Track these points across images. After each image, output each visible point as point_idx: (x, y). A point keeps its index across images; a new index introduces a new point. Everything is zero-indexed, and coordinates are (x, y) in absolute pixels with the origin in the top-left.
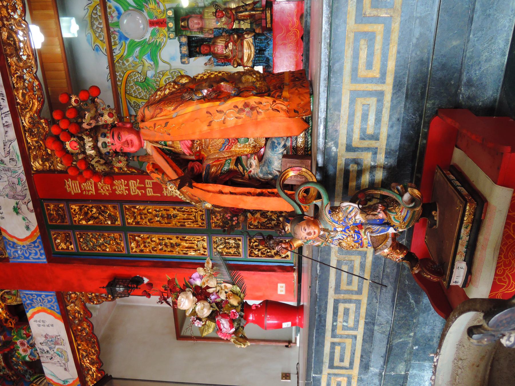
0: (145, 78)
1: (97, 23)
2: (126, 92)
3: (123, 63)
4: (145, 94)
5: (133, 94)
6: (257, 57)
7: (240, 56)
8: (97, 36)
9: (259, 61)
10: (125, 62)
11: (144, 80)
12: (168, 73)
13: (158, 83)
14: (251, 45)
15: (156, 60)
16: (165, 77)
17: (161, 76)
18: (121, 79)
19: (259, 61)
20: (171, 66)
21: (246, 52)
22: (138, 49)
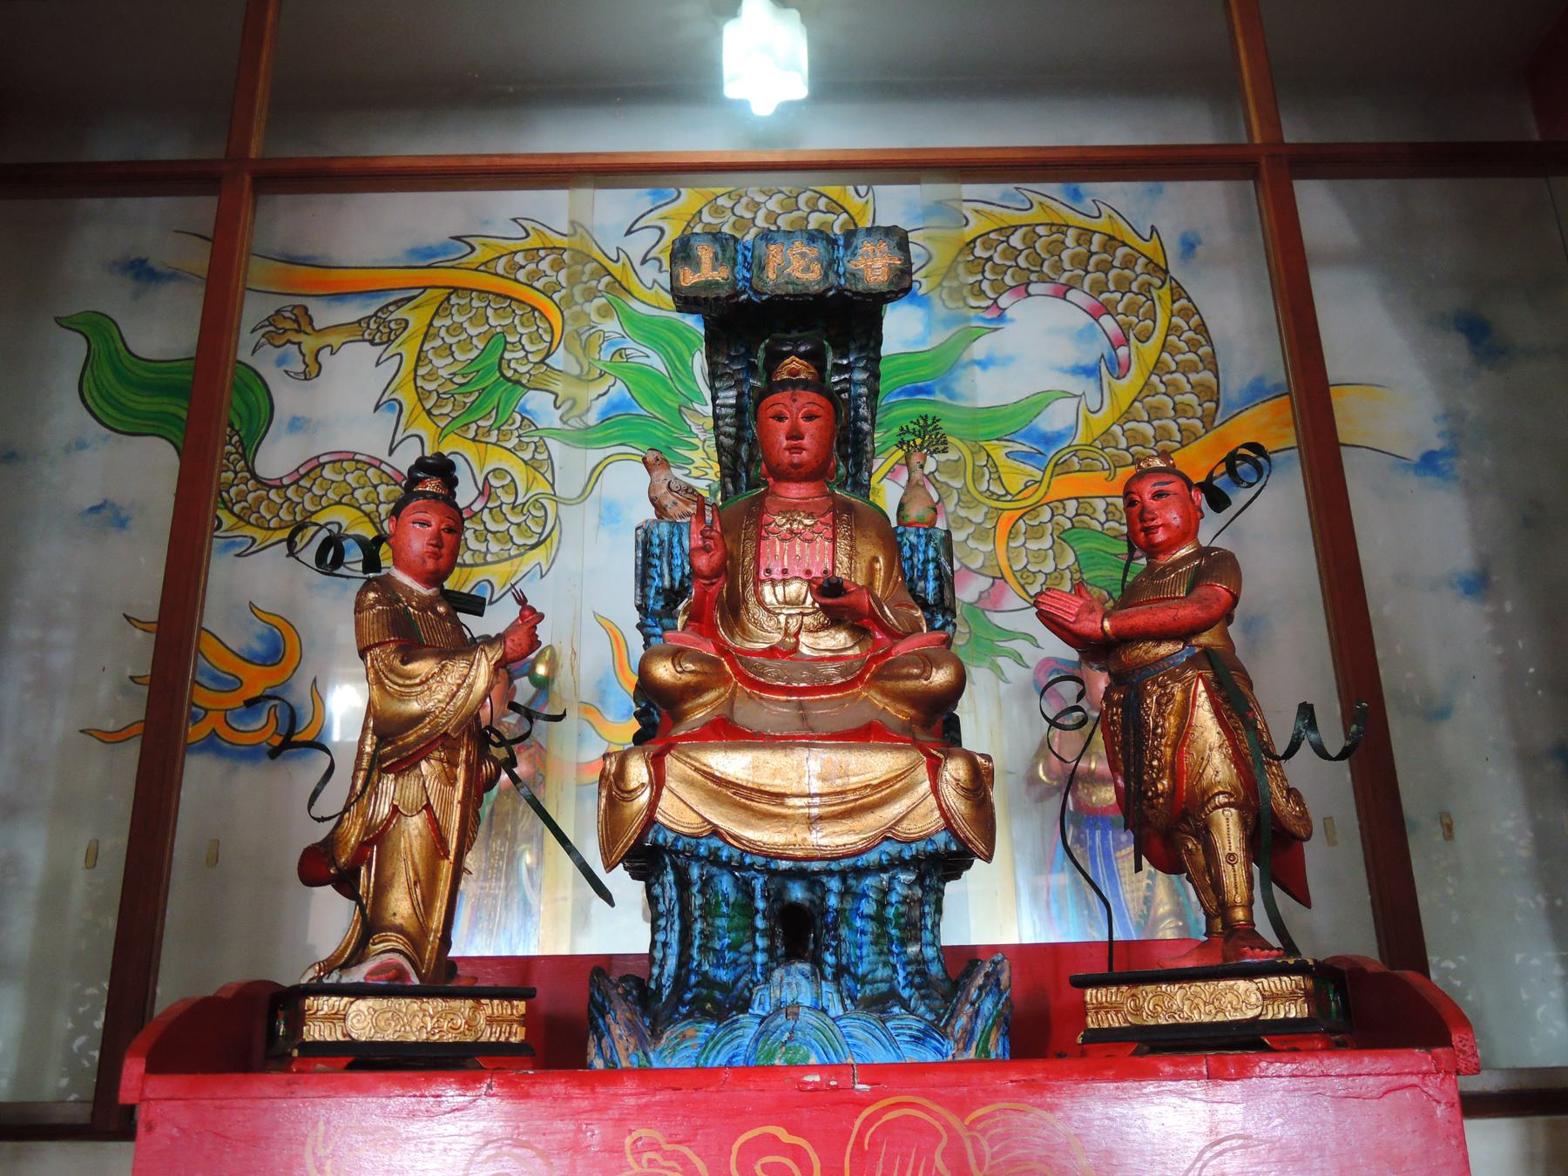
0: (518, 382)
1: (773, 205)
2: (455, 290)
3: (591, 295)
4: (444, 373)
5: (448, 322)
6: (745, 888)
7: (748, 714)
8: (720, 201)
9: (709, 911)
10: (599, 302)
11: (509, 373)
12: (541, 487)
13: (493, 438)
14: (874, 822)
15: (605, 439)
16: (519, 473)
17: (527, 456)
18: (521, 275)
19: (709, 911)
20: (568, 502)
21: (804, 771)
22: (656, 362)
